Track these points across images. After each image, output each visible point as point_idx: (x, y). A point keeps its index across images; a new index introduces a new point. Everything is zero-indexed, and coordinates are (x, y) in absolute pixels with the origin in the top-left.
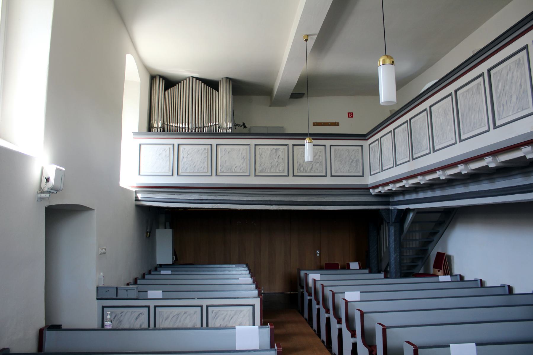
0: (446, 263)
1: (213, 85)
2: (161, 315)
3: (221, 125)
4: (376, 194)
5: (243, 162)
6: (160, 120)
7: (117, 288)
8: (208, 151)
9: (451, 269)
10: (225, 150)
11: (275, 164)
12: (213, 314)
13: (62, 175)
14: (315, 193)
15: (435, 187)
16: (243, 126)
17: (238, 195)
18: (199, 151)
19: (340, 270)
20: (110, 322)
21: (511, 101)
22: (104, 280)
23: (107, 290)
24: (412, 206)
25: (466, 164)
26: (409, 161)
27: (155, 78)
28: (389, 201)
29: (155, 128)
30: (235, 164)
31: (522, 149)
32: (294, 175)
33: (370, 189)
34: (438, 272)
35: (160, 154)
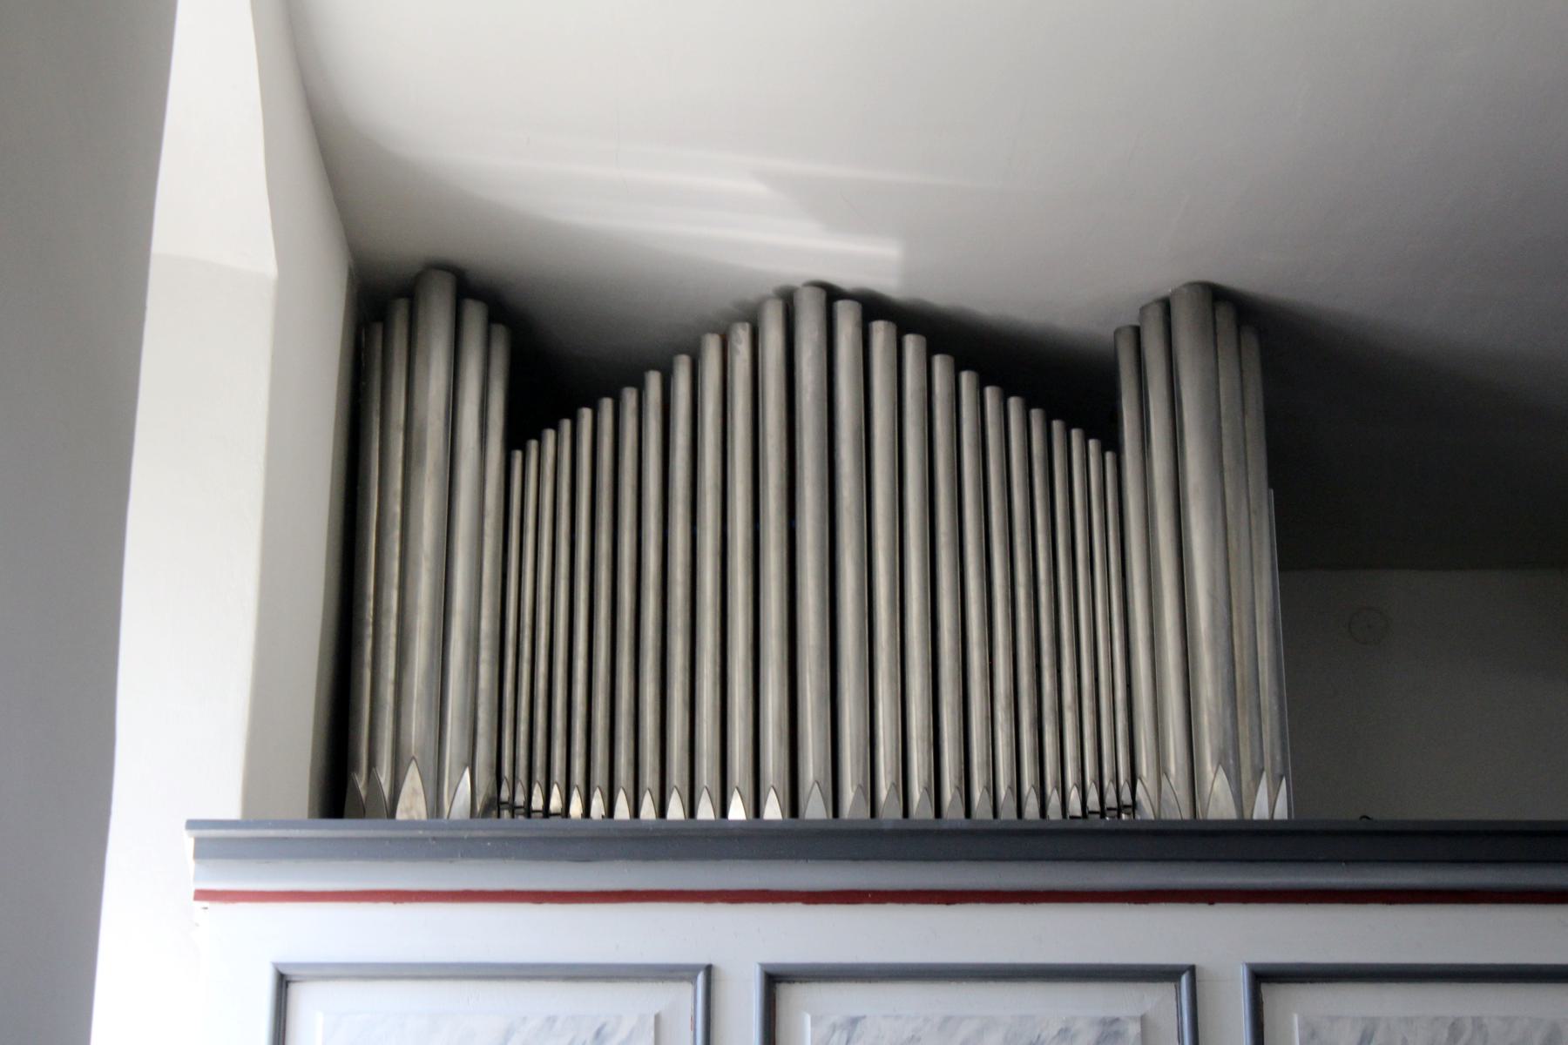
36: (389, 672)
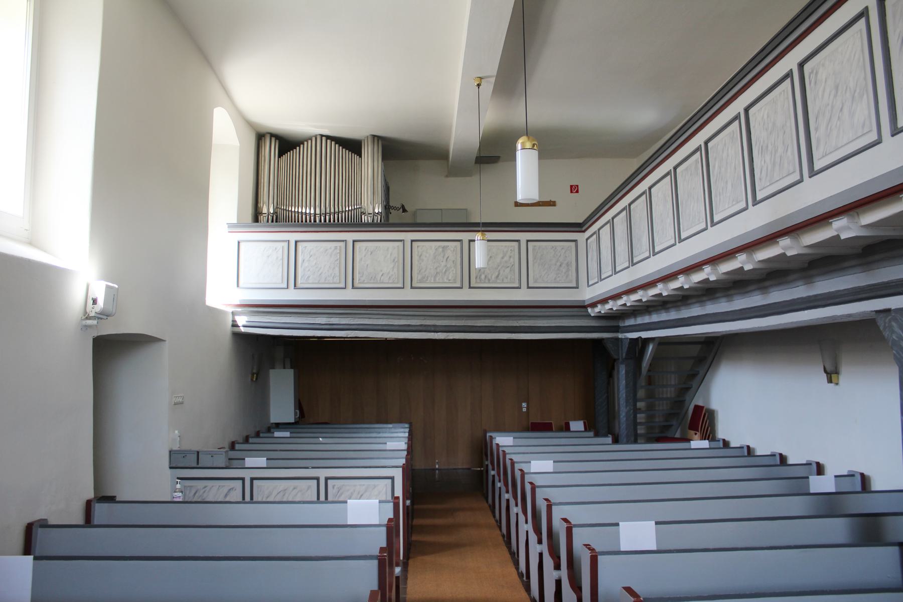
0: (705, 421)
1: (353, 146)
2: (260, 491)
3: (365, 209)
4: (606, 312)
5: (393, 268)
6: (272, 202)
7: (198, 452)
8: (340, 250)
10: (366, 249)
11: (442, 270)
13: (114, 295)
15: (669, 306)
18: (327, 250)
20: (181, 494)
21: (727, 188)
22: (180, 441)
23: (184, 455)
24: (645, 335)
26: (628, 267)
27: (263, 138)
30: (381, 271)
32: (471, 286)
33: (588, 307)
35: (268, 257)
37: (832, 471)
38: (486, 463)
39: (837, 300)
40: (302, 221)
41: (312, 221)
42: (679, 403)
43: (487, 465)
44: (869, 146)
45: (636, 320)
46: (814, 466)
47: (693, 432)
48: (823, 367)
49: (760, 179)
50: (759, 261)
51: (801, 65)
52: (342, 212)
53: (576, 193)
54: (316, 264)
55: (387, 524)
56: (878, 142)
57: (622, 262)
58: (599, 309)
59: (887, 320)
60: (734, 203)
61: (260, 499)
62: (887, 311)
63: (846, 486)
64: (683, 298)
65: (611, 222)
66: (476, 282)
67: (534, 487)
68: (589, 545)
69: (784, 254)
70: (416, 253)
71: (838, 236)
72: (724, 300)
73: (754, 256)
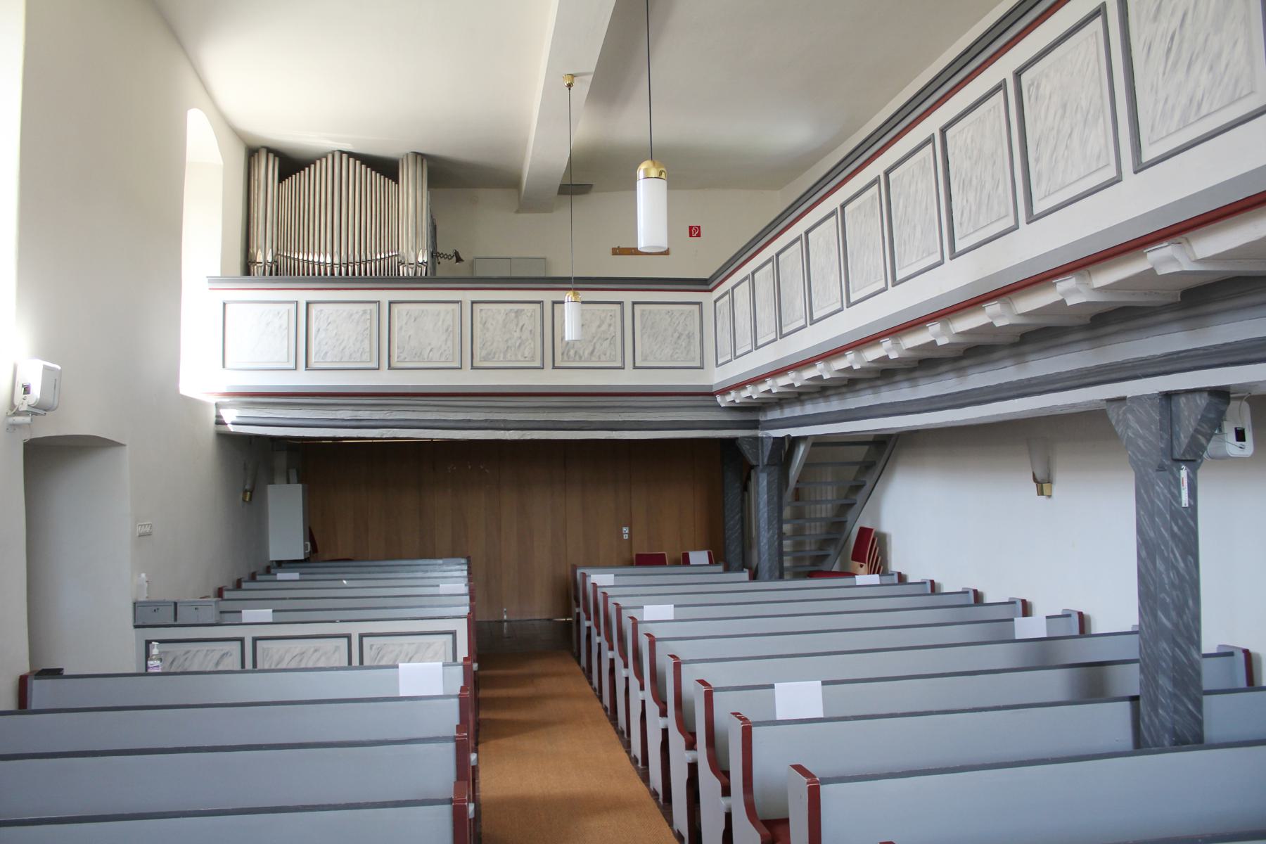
1: (386, 168)
2: (267, 655)
3: (403, 257)
4: (742, 401)
5: (446, 340)
7: (176, 604)
8: (371, 316)
9: (885, 561)
10: (408, 313)
11: (515, 343)
12: (374, 652)
14: (600, 404)
15: (829, 392)
16: (455, 258)
17: (436, 409)
18: (351, 315)
19: (669, 566)
20: (159, 662)
21: (914, 236)
22: (148, 588)
23: (155, 608)
24: (795, 432)
25: (859, 351)
28: (758, 421)
29: (258, 265)
30: (430, 344)
31: (930, 328)
34: (859, 568)
36: (256, 230)
37: (1041, 610)
38: (577, 610)
39: (1058, 386)
40: (314, 274)
41: (329, 274)
42: (838, 525)
43: (578, 614)
44: (1105, 185)
45: (782, 412)
46: (1020, 605)
47: (857, 564)
48: (1032, 475)
49: (961, 224)
50: (958, 333)
51: (1018, 74)
52: (384, 258)
53: (697, 236)
54: (336, 334)
55: (460, 695)
56: (1117, 180)
57: (765, 333)
58: (733, 396)
59: (1121, 412)
60: (924, 255)
61: (266, 667)
62: (1122, 400)
63: (1061, 629)
64: (851, 383)
65: (751, 277)
66: (563, 361)
67: (652, 641)
68: (739, 714)
69: (991, 324)
70: (479, 319)
71: (1063, 302)
72: (906, 384)
73: (951, 326)
